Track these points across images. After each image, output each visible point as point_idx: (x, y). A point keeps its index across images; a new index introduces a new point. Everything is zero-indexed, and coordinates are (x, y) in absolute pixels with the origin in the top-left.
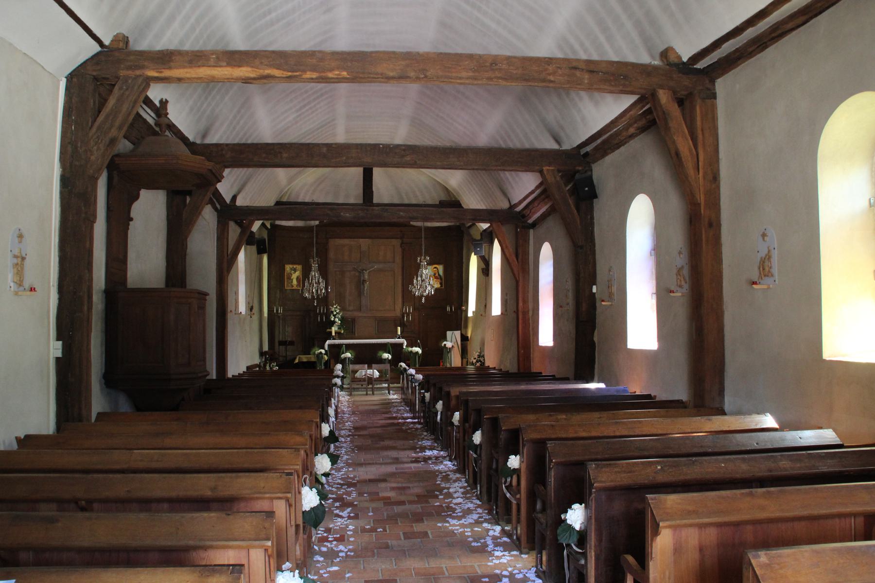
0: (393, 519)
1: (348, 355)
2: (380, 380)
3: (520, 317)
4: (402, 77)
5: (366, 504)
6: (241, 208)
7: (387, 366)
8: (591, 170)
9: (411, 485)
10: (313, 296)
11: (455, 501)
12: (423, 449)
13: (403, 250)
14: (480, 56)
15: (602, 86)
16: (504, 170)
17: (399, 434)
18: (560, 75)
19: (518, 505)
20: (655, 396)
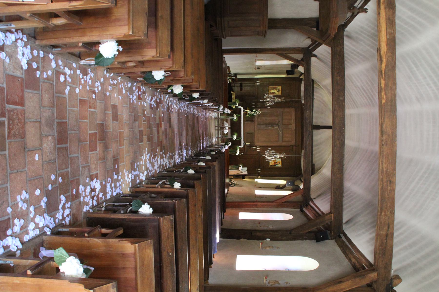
0: (149, 126)
1: (235, 118)
2: (223, 133)
3: (255, 203)
4: (382, 132)
5: (158, 114)
6: (310, 60)
7: (229, 137)
8: (332, 240)
9: (168, 139)
10: (265, 99)
11: (159, 159)
12: (187, 149)
13: (289, 146)
14: (395, 175)
15: (378, 242)
16: (331, 195)
17: (195, 140)
18: (384, 218)
19: (155, 187)
20: (211, 267)
